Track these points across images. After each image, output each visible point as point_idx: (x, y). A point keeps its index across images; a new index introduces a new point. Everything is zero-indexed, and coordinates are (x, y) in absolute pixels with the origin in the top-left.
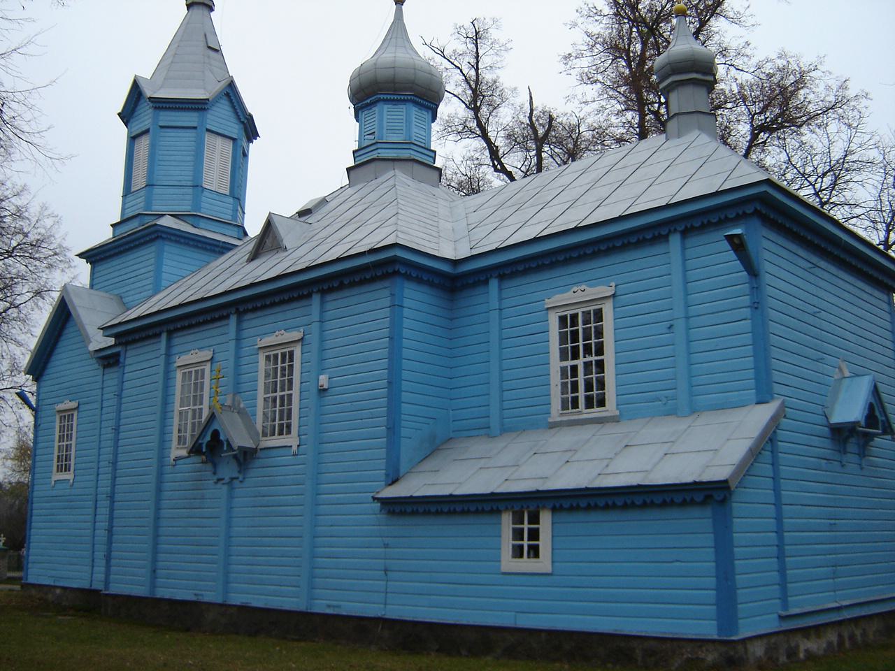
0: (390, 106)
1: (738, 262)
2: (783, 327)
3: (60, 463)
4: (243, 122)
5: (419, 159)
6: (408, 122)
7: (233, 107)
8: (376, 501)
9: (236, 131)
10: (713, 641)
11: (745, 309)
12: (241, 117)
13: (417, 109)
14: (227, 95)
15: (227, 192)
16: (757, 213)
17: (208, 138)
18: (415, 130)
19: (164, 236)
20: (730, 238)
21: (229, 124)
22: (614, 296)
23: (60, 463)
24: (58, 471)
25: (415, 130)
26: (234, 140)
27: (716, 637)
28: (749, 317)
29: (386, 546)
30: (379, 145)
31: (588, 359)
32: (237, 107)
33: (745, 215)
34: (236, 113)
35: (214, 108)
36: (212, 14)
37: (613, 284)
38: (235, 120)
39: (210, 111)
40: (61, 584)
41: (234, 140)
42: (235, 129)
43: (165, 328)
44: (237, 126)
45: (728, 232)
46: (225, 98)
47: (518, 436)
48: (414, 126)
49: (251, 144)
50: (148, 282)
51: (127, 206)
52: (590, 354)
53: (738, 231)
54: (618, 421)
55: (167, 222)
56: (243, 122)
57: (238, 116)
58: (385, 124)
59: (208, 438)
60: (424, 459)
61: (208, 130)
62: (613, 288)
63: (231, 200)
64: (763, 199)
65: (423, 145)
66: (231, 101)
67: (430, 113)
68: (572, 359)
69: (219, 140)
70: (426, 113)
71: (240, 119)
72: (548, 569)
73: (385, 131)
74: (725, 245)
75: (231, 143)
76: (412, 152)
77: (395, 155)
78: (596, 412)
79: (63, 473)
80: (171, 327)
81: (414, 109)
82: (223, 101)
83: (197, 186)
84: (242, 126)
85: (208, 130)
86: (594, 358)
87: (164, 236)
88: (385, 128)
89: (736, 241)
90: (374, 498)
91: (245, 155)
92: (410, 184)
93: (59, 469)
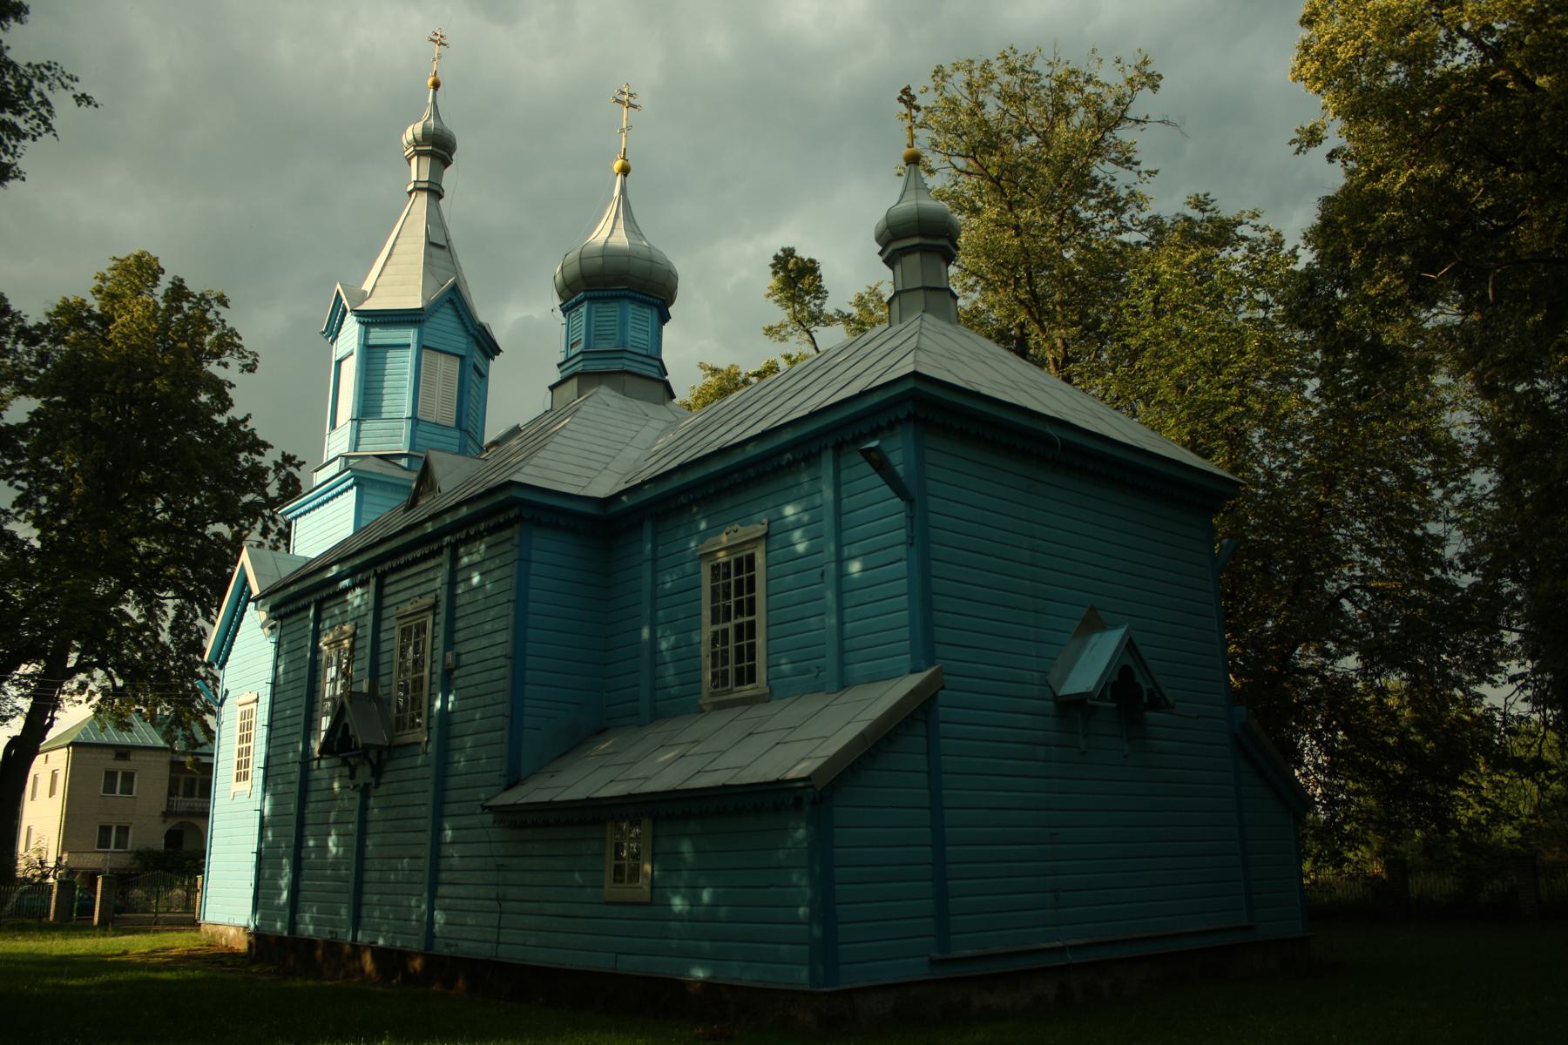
0: (599, 305)
1: (887, 487)
2: (963, 568)
4: (472, 335)
5: (647, 373)
6: (624, 324)
7: (460, 317)
8: (486, 811)
9: (464, 346)
10: (805, 993)
11: (899, 547)
12: (470, 328)
13: (634, 307)
14: (451, 301)
15: (452, 423)
16: (910, 418)
18: (633, 334)
19: (683, 500)
20: (867, 454)
21: (455, 338)
22: (767, 536)
25: (633, 334)
27: (807, 988)
28: (904, 557)
29: (500, 867)
30: (626, 355)
31: (740, 620)
32: (464, 317)
33: (891, 426)
34: (464, 324)
35: (434, 319)
36: (441, 202)
37: (765, 521)
38: (462, 333)
39: (427, 324)
42: (461, 343)
43: (312, 598)
44: (464, 340)
45: (867, 443)
46: (448, 305)
47: (697, 721)
48: (630, 328)
49: (491, 362)
52: (742, 615)
53: (874, 444)
54: (768, 701)
56: (472, 335)
57: (466, 327)
58: (593, 328)
59: (339, 735)
60: (561, 755)
62: (766, 526)
63: (457, 434)
64: (914, 397)
65: (644, 352)
66: (456, 310)
67: (655, 312)
68: (742, 624)
69: (442, 358)
70: (649, 311)
71: (468, 331)
72: (647, 897)
73: (592, 337)
74: (861, 458)
76: (626, 362)
77: (602, 367)
78: (748, 690)
79: (242, 782)
80: (317, 596)
81: (631, 306)
82: (443, 310)
84: (471, 339)
86: (746, 619)
88: (593, 334)
89: (874, 455)
90: (484, 808)
91: (483, 376)
92: (609, 402)
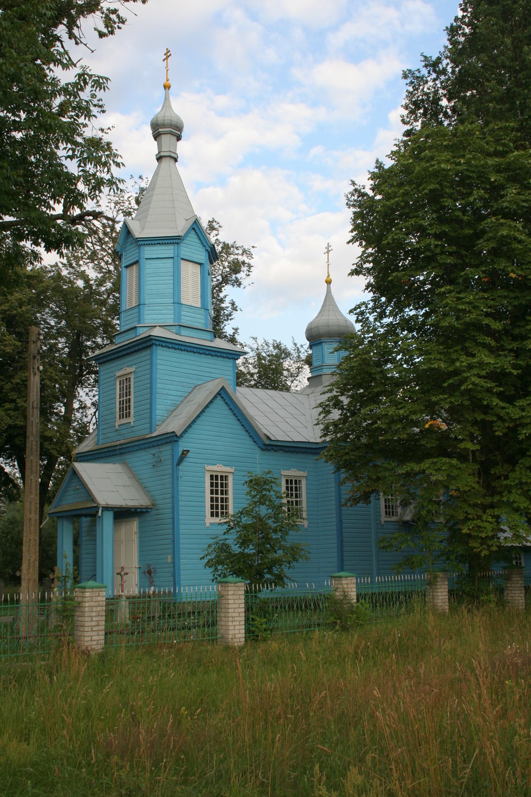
3: (121, 399)
15: (199, 306)
17: (183, 264)
23: (121, 399)
24: (120, 418)
26: (200, 264)
40: (39, 393)
41: (200, 264)
50: (191, 239)
51: (137, 255)
55: (157, 332)
56: (207, 250)
61: (182, 259)
69: (190, 265)
71: (202, 244)
75: (199, 266)
83: (178, 303)
85: (182, 259)
86: (214, 496)
87: (157, 343)
93: (121, 417)
